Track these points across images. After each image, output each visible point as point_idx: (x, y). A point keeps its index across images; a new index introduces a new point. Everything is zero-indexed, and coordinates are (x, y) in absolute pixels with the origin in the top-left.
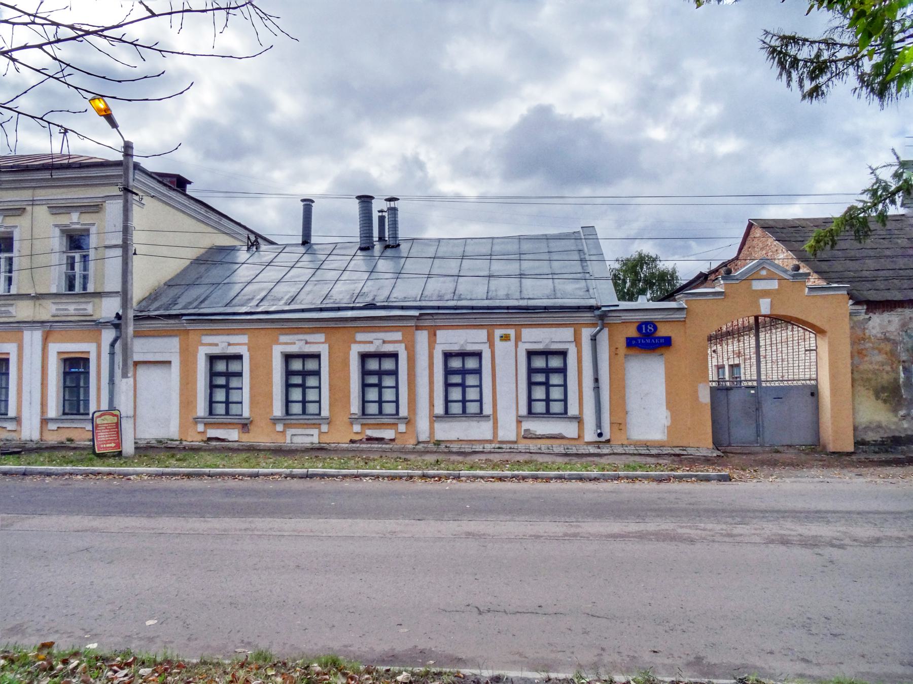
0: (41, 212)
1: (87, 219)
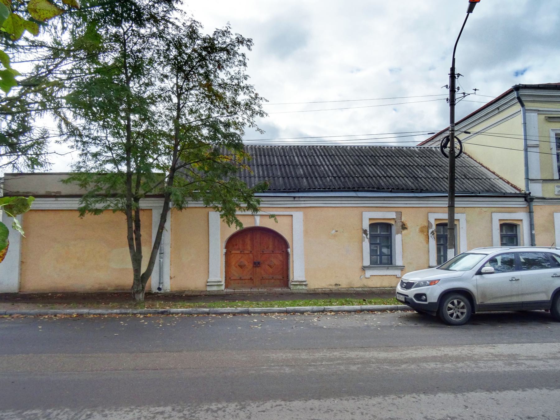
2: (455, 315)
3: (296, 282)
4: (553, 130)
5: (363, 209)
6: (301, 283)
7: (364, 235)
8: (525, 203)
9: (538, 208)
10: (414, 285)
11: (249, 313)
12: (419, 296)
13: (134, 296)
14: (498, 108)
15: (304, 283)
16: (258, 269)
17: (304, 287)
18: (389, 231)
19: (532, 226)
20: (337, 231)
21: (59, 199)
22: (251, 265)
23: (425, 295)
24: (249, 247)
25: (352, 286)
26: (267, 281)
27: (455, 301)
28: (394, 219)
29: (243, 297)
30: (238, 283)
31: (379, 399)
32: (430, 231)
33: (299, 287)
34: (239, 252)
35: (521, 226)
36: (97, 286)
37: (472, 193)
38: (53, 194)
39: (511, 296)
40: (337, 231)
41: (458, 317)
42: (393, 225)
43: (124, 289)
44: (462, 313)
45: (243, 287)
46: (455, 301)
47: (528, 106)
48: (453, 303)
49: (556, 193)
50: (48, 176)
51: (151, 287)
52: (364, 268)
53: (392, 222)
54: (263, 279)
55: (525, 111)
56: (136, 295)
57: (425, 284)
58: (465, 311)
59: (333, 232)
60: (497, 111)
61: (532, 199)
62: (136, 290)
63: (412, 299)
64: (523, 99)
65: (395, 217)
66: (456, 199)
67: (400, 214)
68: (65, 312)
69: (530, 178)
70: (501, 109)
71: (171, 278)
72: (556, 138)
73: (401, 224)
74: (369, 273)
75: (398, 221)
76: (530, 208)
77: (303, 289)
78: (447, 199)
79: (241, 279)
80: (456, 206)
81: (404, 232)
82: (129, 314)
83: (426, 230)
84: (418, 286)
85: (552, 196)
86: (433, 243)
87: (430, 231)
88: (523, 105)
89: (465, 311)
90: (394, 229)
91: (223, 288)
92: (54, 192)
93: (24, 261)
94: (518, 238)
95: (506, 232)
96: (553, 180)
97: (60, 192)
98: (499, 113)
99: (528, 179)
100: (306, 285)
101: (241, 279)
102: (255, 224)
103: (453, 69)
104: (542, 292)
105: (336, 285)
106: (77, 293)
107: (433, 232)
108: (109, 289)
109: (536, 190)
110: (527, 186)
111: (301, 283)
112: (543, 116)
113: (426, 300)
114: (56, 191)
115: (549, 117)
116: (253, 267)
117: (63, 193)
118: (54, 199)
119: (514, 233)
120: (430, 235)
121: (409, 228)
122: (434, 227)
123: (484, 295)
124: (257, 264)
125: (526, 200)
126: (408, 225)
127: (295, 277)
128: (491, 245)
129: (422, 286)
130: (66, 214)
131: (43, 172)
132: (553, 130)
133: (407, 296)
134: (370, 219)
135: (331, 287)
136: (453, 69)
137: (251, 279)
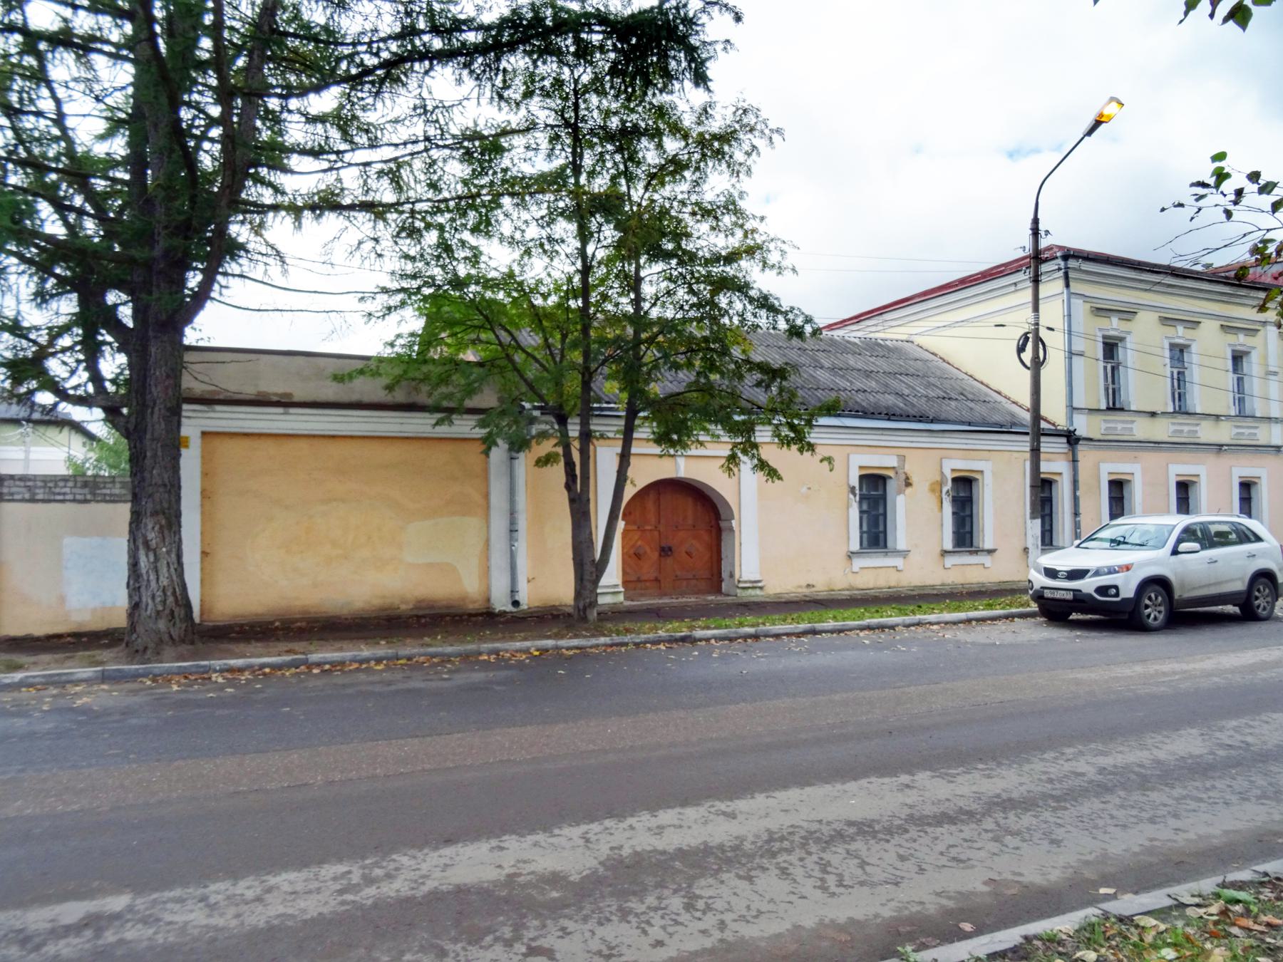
0: (1209, 329)
1: (1190, 334)
2: (1152, 616)
3: (746, 582)
4: (1100, 330)
5: (849, 449)
6: (755, 585)
7: (851, 496)
8: (1066, 446)
9: (1083, 452)
10: (1089, 574)
11: (814, 632)
12: (1102, 590)
13: (585, 613)
14: (1015, 284)
15: (760, 585)
16: (669, 561)
17: (758, 592)
18: (881, 487)
19: (1075, 483)
20: (809, 488)
21: (292, 410)
22: (657, 554)
23: (1116, 587)
24: (652, 517)
25: (832, 587)
26: (685, 583)
27: (1153, 595)
28: (894, 468)
29: (657, 614)
30: (635, 589)
31: (760, 799)
32: (945, 490)
33: (750, 592)
34: (635, 528)
35: (1060, 483)
36: (377, 602)
37: (1001, 426)
38: (275, 399)
39: (1209, 585)
40: (809, 488)
41: (1155, 619)
42: (891, 478)
43: (432, 607)
44: (1160, 612)
45: (642, 595)
46: (1153, 595)
47: (1074, 287)
48: (1150, 599)
49: (1103, 432)
50: (262, 356)
51: (488, 600)
52: (945, 553)
53: (891, 473)
54: (677, 578)
55: (1070, 295)
56: (588, 611)
57: (1111, 571)
58: (1162, 608)
59: (804, 489)
60: (1013, 288)
61: (1078, 440)
62: (588, 601)
63: (1090, 595)
64: (1071, 275)
65: (895, 464)
66: (1043, 439)
67: (902, 459)
68: (513, 648)
69: (1075, 405)
70: (1019, 286)
71: (529, 581)
72: (1104, 343)
73: (903, 477)
74: (858, 563)
75: (900, 471)
76: (1074, 455)
77: (757, 596)
78: (1027, 438)
79: (639, 580)
80: (1042, 450)
81: (909, 490)
82: (626, 644)
83: (938, 488)
84: (1097, 573)
85: (1098, 436)
86: (948, 509)
87: (945, 490)
88: (1067, 285)
89: (1162, 608)
90: (891, 486)
91: (621, 598)
92: (276, 394)
93: (208, 551)
94: (1054, 503)
95: (868, 489)
96: (1098, 410)
97: (290, 395)
98: (1016, 291)
99: (1072, 409)
100: (761, 588)
101: (639, 580)
102: (677, 472)
103: (1036, 221)
104: (1237, 579)
105: (808, 586)
106: (339, 617)
107: (948, 492)
108: (403, 607)
109: (1082, 426)
110: (1071, 419)
111: (755, 585)
112: (1088, 306)
113: (1117, 595)
114: (281, 391)
115: (1098, 309)
116: (660, 555)
117: (297, 398)
118: (280, 410)
119: (880, 492)
120: (944, 496)
121: (914, 484)
122: (949, 485)
123: (1182, 586)
124: (665, 551)
125: (1069, 442)
126: (914, 479)
127: (743, 574)
128: (1168, 512)
129: (1118, 572)
130: (303, 445)
131: (194, 344)
132: (1100, 330)
133: (1080, 591)
134: (861, 468)
135: (800, 590)
136: (1036, 221)
137: (657, 580)
